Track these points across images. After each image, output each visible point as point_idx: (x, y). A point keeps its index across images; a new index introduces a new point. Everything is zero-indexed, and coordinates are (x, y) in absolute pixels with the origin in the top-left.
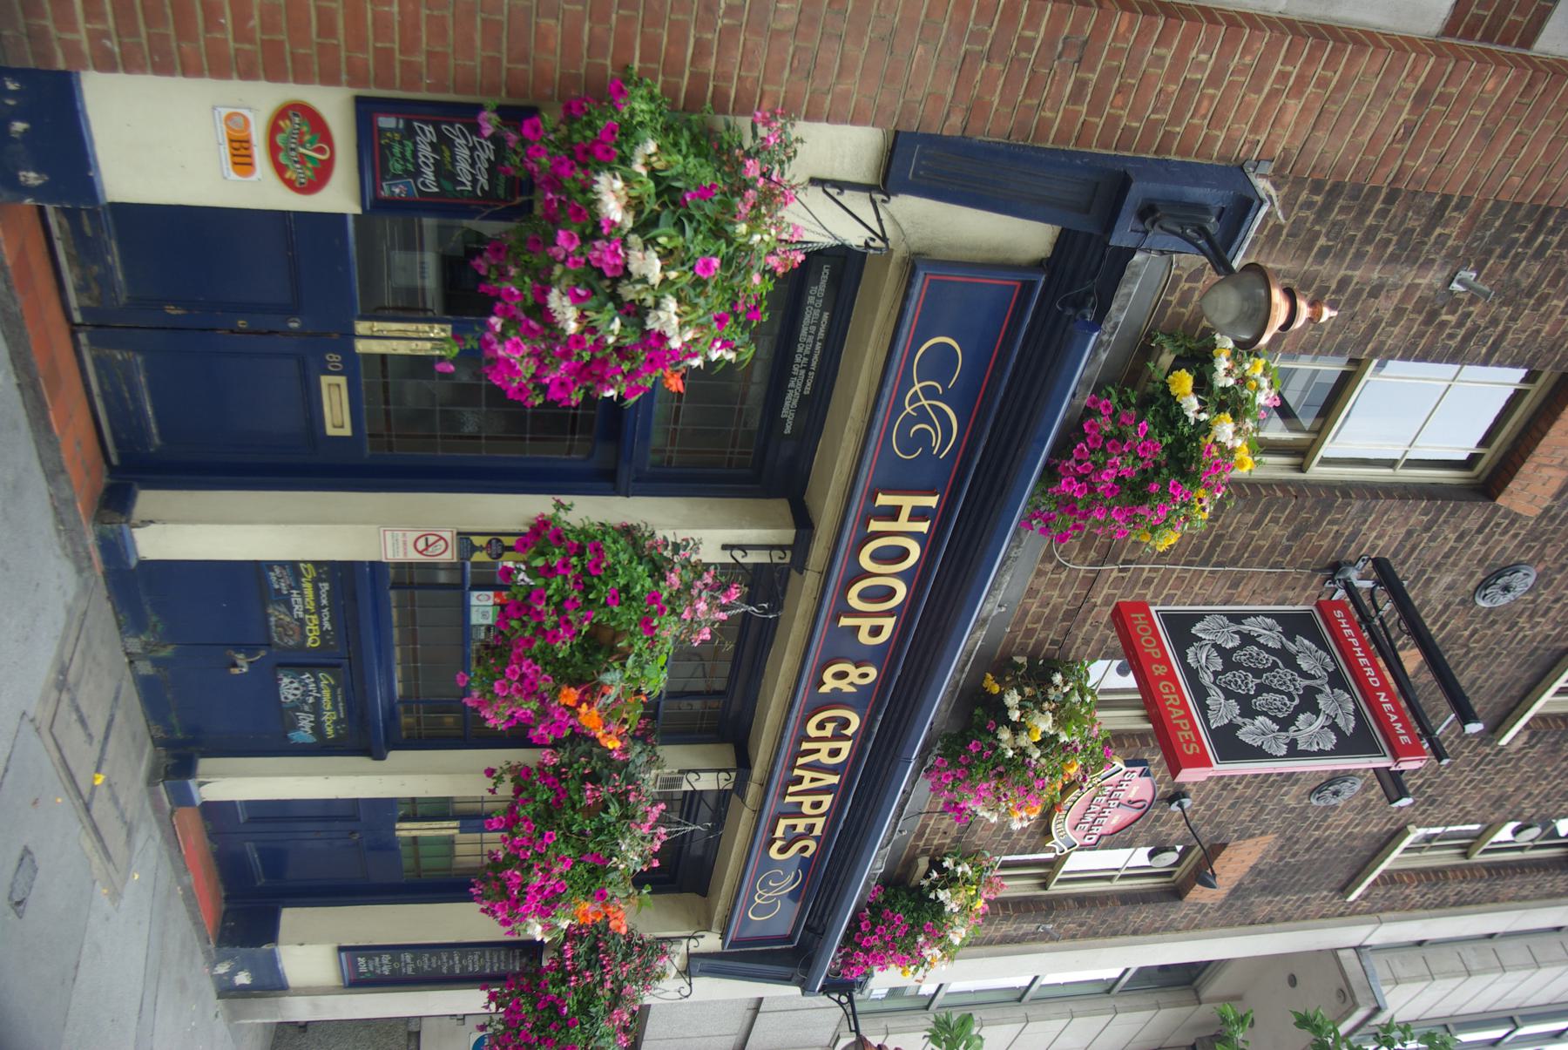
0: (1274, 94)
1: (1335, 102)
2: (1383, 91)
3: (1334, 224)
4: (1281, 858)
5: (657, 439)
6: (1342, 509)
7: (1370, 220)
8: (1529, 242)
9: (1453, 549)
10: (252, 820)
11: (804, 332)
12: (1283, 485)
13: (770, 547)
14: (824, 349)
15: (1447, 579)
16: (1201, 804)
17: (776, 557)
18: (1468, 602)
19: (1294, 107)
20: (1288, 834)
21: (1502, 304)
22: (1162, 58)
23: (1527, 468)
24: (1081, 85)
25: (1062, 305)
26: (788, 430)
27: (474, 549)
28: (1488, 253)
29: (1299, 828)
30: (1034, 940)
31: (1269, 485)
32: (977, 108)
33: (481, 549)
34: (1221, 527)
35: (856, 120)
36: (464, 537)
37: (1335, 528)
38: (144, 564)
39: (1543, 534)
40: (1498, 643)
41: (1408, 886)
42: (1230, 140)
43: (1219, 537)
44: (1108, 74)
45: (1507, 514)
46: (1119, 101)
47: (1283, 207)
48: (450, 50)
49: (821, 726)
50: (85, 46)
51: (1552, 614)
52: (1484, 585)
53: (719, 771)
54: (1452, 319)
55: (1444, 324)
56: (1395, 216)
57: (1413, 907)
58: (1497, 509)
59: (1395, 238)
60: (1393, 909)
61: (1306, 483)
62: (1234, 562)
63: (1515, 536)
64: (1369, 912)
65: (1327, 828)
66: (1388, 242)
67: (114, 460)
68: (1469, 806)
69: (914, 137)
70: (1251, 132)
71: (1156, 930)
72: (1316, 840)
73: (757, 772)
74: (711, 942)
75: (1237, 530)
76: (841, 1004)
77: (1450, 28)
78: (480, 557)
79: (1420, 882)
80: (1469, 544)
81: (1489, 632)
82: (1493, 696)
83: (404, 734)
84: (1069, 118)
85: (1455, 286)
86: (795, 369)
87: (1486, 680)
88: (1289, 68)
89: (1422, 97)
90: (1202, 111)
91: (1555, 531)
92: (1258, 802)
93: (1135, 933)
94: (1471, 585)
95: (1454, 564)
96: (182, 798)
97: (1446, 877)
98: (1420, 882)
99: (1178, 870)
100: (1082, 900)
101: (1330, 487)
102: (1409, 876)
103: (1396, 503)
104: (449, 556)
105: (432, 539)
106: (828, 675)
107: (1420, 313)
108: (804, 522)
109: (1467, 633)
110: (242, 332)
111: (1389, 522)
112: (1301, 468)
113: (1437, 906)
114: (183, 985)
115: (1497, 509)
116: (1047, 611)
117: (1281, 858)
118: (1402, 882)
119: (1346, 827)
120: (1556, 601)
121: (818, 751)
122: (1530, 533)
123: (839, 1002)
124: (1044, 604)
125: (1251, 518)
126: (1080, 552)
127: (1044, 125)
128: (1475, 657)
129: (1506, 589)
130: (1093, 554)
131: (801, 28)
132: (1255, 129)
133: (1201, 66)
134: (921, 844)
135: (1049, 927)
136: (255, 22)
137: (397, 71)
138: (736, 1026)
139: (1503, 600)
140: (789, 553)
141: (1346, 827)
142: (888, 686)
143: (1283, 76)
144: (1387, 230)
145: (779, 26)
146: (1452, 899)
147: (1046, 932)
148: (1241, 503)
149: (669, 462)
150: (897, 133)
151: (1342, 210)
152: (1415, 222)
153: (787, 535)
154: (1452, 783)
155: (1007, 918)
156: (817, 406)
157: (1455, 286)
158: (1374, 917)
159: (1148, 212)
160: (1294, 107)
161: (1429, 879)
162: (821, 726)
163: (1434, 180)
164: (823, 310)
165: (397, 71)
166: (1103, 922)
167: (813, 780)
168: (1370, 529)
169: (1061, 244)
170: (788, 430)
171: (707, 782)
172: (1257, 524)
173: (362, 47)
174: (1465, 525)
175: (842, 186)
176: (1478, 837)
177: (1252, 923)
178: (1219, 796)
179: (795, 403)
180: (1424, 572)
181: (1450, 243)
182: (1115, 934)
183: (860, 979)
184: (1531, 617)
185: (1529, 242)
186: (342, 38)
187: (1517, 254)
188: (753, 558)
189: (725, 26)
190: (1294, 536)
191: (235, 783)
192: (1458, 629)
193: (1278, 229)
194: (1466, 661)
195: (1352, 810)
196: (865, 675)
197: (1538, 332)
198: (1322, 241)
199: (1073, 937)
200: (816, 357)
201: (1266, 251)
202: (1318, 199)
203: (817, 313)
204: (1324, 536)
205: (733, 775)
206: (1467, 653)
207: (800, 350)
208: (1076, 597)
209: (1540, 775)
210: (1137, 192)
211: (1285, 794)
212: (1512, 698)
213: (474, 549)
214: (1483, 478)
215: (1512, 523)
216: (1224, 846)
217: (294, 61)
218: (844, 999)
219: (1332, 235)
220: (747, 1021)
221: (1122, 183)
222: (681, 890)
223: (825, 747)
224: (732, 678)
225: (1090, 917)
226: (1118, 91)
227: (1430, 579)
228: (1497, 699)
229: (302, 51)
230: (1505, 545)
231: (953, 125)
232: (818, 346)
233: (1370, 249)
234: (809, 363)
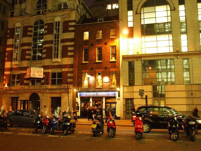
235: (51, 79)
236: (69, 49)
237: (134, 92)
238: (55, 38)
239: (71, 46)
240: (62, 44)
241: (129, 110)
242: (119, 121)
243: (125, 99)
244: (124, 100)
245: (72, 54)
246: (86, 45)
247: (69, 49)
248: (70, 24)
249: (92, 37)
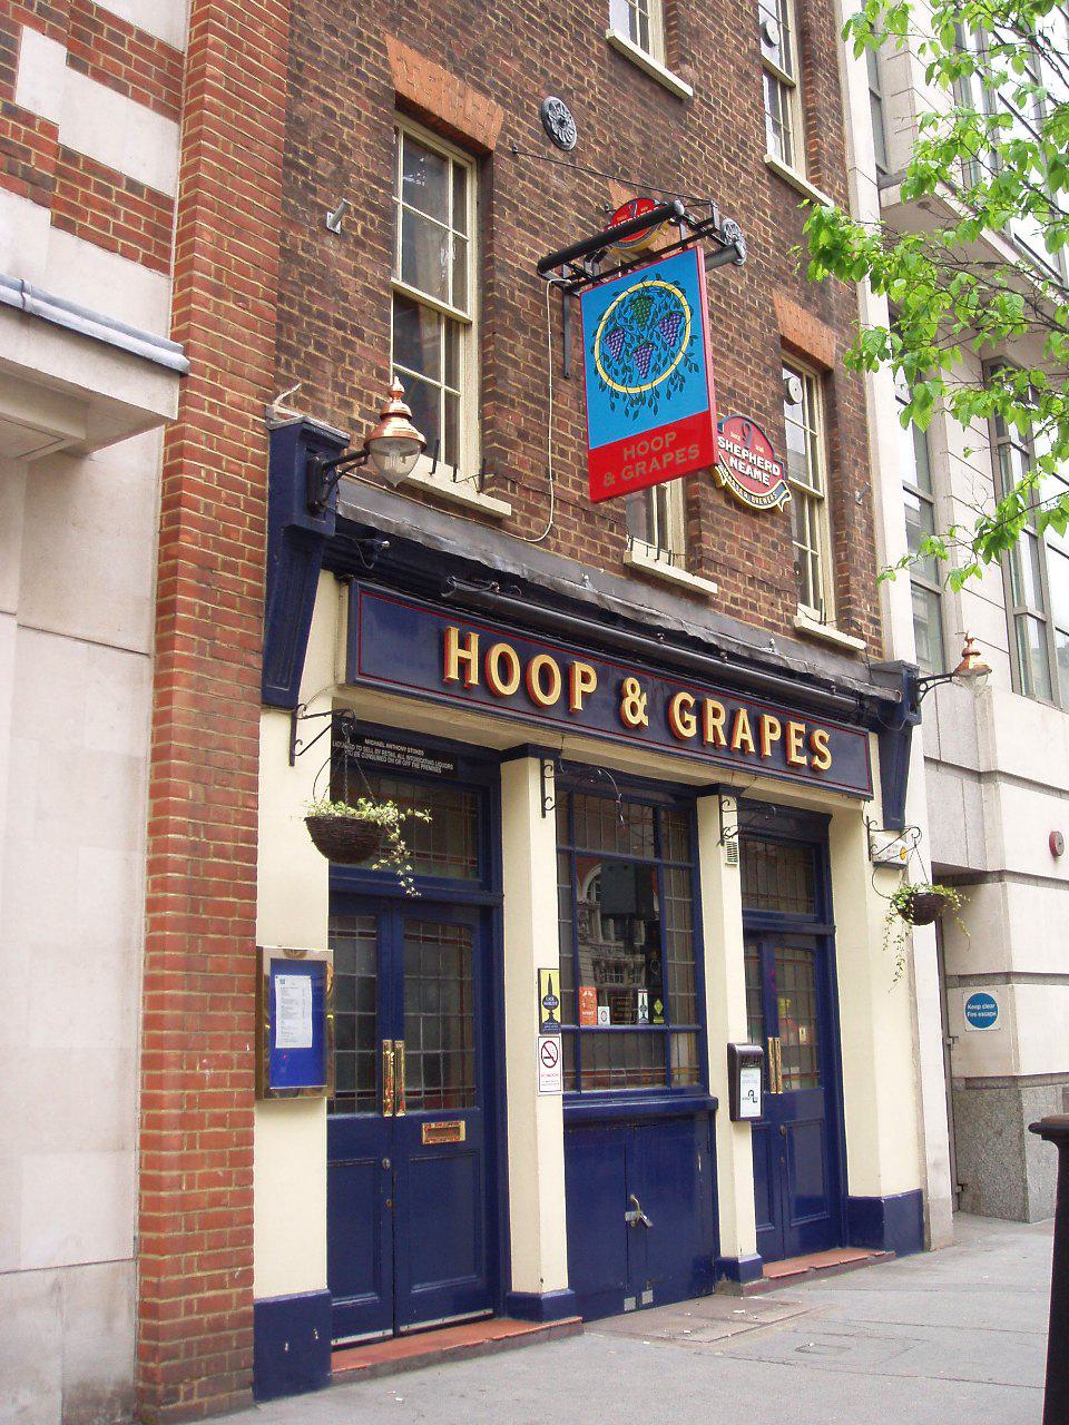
0: (224, 413)
1: (226, 363)
2: (215, 325)
3: (299, 342)
4: (795, 280)
5: (454, 873)
6: (502, 290)
7: (296, 312)
8: (304, 171)
9: (532, 181)
10: (771, 1219)
11: (379, 758)
12: (483, 343)
13: (543, 777)
14: (391, 742)
15: (555, 179)
16: (745, 369)
17: (549, 773)
18: (573, 155)
19: (231, 395)
20: (772, 279)
21: (348, 184)
22: (206, 505)
23: (467, 129)
25: (369, 563)
26: (449, 766)
27: (551, 1019)
28: (314, 204)
29: (768, 270)
30: (870, 507)
31: (483, 357)
32: (244, 642)
33: (551, 1014)
34: (518, 395)
35: (255, 734)
36: (544, 1029)
37: (517, 293)
38: (571, 1285)
39: (516, 98)
40: (605, 116)
41: (820, 147)
42: (255, 443)
43: (528, 397)
44: (219, 547)
45: (503, 137)
46: (234, 535)
47: (290, 387)
48: (229, 1033)
49: (686, 725)
50: (240, 1290)
51: (581, 71)
52: (559, 144)
53: (721, 811)
54: (360, 224)
55: (365, 232)
56: (292, 291)
57: (841, 137)
58: (499, 147)
59: (307, 288)
60: (843, 157)
61: (482, 322)
62: (545, 379)
63: (519, 125)
64: (845, 181)
65: (766, 241)
66: (310, 293)
67: (489, 1311)
68: (747, 105)
69: (264, 691)
70: (247, 427)
71: (861, 389)
72: (778, 250)
73: (721, 779)
74: (873, 809)
75: (520, 382)
76: (928, 689)
77: (155, 263)
78: (557, 1015)
79: (817, 135)
80: (527, 166)
81: (597, 127)
82: (650, 108)
83: (695, 1083)
84: (247, 572)
85: (338, 229)
86: (407, 764)
87: (637, 119)
88: (206, 405)
89: (218, 292)
90: (237, 468)
91: (515, 88)
92: (744, 315)
93: (863, 410)
94: (559, 155)
95: (542, 175)
96: (754, 1269)
97: (813, 109)
98: (817, 135)
99: (805, 373)
100: (834, 464)
101: (485, 301)
102: (812, 146)
103: (496, 242)
104: (557, 1040)
105: (545, 1054)
106: (634, 720)
107: (357, 254)
108: (522, 751)
109: (598, 149)
111: (511, 245)
112: (468, 325)
113: (840, 113)
115: (499, 147)
116: (587, 538)
117: (795, 280)
118: (817, 153)
119: (765, 222)
120: (570, 70)
121: (715, 727)
122: (517, 113)
123: (925, 692)
124: (580, 541)
125: (511, 371)
126: (540, 516)
127: (254, 592)
128: (618, 136)
129: (562, 123)
130: (541, 506)
131: (203, 780)
132: (245, 423)
133: (209, 473)
134: (782, 625)
135: (858, 494)
136: (220, 1171)
137: (244, 1071)
138: (952, 781)
139: (572, 124)
140: (547, 762)
141: (765, 222)
143: (212, 408)
144: (301, 296)
145: (202, 796)
146: (833, 98)
147: (862, 496)
148: (500, 381)
149: (473, 862)
150: (263, 703)
151: (290, 337)
152: (296, 271)
153: (532, 764)
154: (726, 129)
155: (849, 537)
156: (436, 746)
157: (338, 229)
158: (850, 174)
159: (313, 510)
160: (231, 395)
161: (810, 83)
162: (686, 725)
163: (271, 269)
164: (364, 745)
165: (244, 1071)
166: (853, 442)
167: (744, 731)
168: (516, 260)
169: (327, 567)
170: (449, 766)
171: (731, 820)
172: (515, 364)
173: (228, 1096)
174: (512, 174)
175: (293, 741)
176: (773, 76)
177: (855, 296)
178: (739, 354)
179: (431, 762)
180: (550, 202)
181: (308, 240)
182: (864, 430)
183: (904, 672)
184: (584, 91)
185: (304, 171)
186: (226, 1110)
187: (313, 180)
188: (550, 791)
189: (205, 836)
190: (523, 328)
191: (739, 1233)
192: (595, 159)
193: (306, 389)
194: (621, 144)
195: (750, 221)
196: (633, 687)
197: (366, 145)
198: (311, 349)
199: (867, 469)
200: (397, 747)
201: (320, 395)
202: (283, 358)
203: (366, 749)
204: (523, 302)
205: (724, 798)
206: (614, 144)
207: (392, 761)
208: (575, 515)
209: (720, 42)
210: (300, 519)
211: (736, 289)
212: (652, 90)
213: (551, 1019)
214: (471, 159)
215: (509, 130)
216: (783, 339)
217: (242, 1145)
218: (923, 687)
219: (306, 341)
220: (949, 770)
221: (294, 531)
222: (826, 839)
223: (711, 721)
224: (644, 802)
225: (849, 455)
226: (228, 536)
227: (556, 196)
228: (652, 104)
229: (235, 1139)
230: (527, 132)
231: (257, 661)
232: (389, 746)
233: (315, 307)
234: (401, 752)
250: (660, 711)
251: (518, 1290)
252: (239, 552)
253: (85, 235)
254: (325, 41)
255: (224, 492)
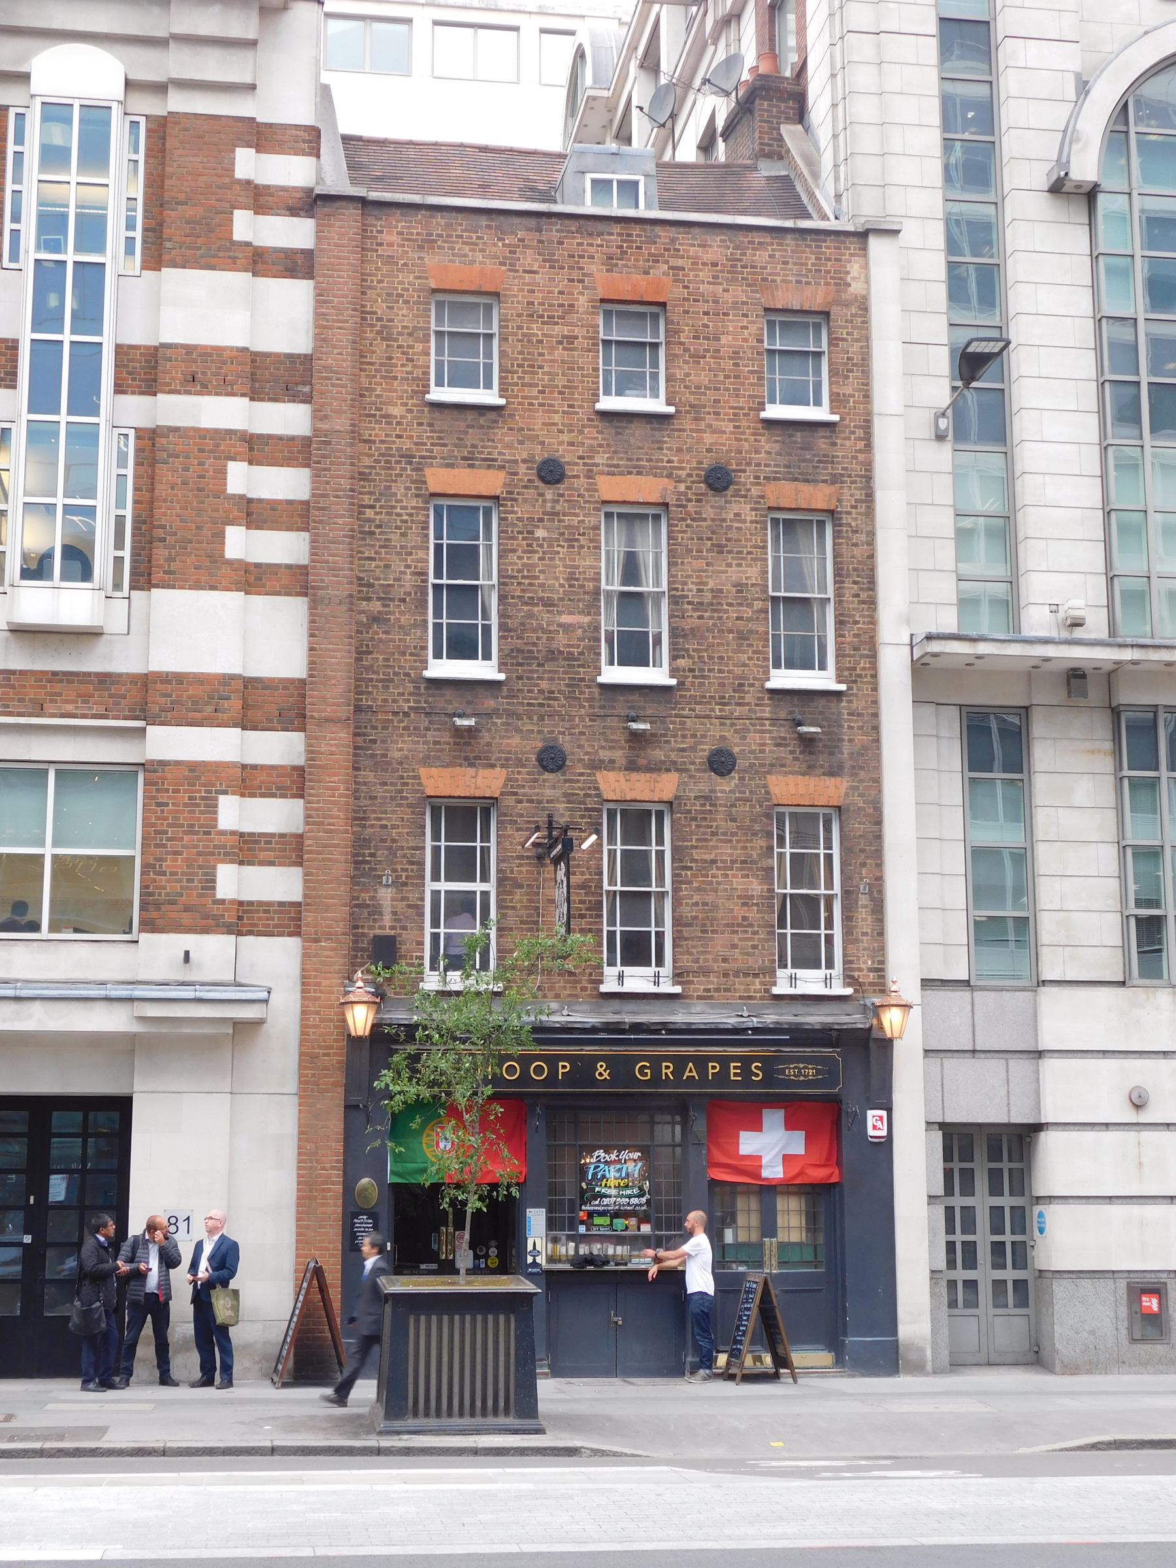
0: (321, 992)
2: (316, 955)
19: (324, 983)
24: (324, 1055)
32: (335, 1084)
44: (320, 1047)
84: (335, 1054)
110: (11, 1171)
114: (169, 1260)
142: (37, 1438)
160: (324, 983)
172: (513, 908)
204: (520, 872)
231: (341, 1090)
235: (33, 255)
236: (234, 814)
237: (1040, 1054)
238: (45, 317)
239: (250, 781)
240: (139, 411)
241: (999, 1285)
242: (922, 1536)
243: (943, 1126)
244: (938, 1136)
245: (282, 547)
246: (469, 461)
247: (234, 814)
248: (248, 164)
249: (541, 378)
250: (656, 1071)
251: (51, 1182)
252: (331, 1047)
253: (260, 934)
254: (379, 791)
255: (322, 1025)
